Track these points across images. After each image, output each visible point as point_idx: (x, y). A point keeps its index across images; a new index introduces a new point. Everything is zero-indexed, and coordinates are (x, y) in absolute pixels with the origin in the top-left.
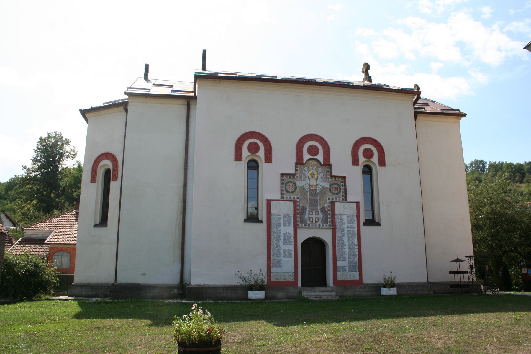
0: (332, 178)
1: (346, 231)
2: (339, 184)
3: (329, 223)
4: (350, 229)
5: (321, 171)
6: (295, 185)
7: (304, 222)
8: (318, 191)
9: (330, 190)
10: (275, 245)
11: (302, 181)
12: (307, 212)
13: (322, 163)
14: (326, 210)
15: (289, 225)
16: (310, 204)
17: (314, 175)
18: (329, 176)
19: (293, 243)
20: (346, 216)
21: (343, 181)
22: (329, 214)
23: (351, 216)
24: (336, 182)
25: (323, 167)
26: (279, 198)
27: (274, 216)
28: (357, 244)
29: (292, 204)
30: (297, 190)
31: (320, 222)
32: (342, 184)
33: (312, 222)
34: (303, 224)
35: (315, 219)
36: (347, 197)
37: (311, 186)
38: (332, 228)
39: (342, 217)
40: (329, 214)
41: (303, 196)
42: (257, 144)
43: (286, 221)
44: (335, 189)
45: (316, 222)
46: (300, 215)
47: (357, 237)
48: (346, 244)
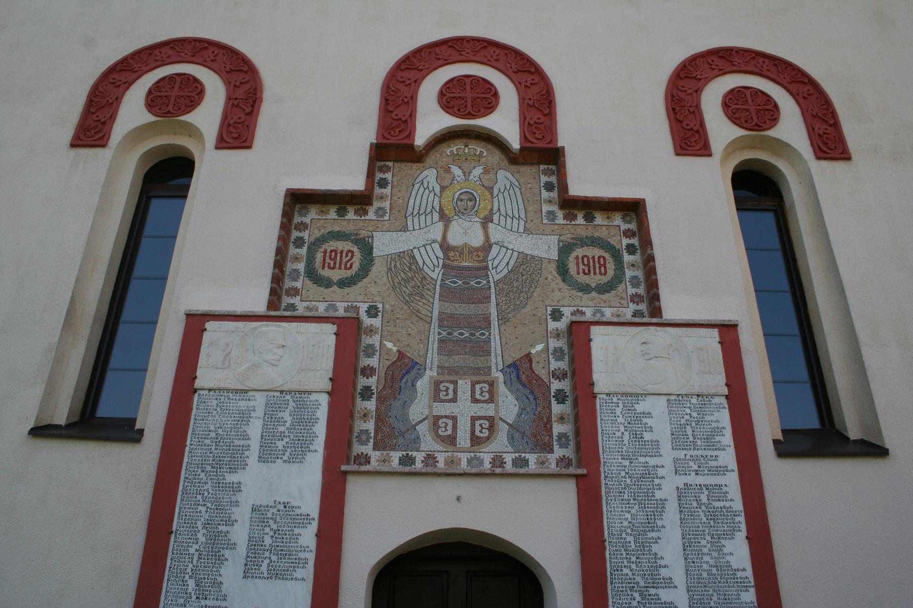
0: (570, 217)
1: (667, 490)
2: (613, 241)
3: (561, 446)
4: (692, 479)
5: (511, 184)
6: (367, 248)
7: (401, 441)
8: (495, 276)
9: (562, 269)
10: (191, 583)
11: (405, 229)
12: (423, 385)
13: (516, 145)
14: (542, 373)
15: (298, 454)
16: (441, 341)
17: (470, 204)
18: (555, 208)
19: (308, 572)
20: (663, 400)
21: (633, 226)
22: (561, 397)
23: (694, 400)
24: (596, 234)
25: (525, 169)
26: (260, 306)
27: (215, 402)
28: (749, 573)
29: (326, 335)
30: (373, 274)
31: (501, 442)
32: (625, 241)
33: (451, 440)
34: (396, 456)
35: (473, 425)
36: (658, 299)
37: (452, 254)
38: (577, 477)
39: (640, 407)
40: (568, 440)
41: (407, 303)
42: (196, 80)
43: (281, 429)
44: (588, 265)
45: (476, 441)
46: (381, 400)
47: (743, 526)
48: (677, 573)
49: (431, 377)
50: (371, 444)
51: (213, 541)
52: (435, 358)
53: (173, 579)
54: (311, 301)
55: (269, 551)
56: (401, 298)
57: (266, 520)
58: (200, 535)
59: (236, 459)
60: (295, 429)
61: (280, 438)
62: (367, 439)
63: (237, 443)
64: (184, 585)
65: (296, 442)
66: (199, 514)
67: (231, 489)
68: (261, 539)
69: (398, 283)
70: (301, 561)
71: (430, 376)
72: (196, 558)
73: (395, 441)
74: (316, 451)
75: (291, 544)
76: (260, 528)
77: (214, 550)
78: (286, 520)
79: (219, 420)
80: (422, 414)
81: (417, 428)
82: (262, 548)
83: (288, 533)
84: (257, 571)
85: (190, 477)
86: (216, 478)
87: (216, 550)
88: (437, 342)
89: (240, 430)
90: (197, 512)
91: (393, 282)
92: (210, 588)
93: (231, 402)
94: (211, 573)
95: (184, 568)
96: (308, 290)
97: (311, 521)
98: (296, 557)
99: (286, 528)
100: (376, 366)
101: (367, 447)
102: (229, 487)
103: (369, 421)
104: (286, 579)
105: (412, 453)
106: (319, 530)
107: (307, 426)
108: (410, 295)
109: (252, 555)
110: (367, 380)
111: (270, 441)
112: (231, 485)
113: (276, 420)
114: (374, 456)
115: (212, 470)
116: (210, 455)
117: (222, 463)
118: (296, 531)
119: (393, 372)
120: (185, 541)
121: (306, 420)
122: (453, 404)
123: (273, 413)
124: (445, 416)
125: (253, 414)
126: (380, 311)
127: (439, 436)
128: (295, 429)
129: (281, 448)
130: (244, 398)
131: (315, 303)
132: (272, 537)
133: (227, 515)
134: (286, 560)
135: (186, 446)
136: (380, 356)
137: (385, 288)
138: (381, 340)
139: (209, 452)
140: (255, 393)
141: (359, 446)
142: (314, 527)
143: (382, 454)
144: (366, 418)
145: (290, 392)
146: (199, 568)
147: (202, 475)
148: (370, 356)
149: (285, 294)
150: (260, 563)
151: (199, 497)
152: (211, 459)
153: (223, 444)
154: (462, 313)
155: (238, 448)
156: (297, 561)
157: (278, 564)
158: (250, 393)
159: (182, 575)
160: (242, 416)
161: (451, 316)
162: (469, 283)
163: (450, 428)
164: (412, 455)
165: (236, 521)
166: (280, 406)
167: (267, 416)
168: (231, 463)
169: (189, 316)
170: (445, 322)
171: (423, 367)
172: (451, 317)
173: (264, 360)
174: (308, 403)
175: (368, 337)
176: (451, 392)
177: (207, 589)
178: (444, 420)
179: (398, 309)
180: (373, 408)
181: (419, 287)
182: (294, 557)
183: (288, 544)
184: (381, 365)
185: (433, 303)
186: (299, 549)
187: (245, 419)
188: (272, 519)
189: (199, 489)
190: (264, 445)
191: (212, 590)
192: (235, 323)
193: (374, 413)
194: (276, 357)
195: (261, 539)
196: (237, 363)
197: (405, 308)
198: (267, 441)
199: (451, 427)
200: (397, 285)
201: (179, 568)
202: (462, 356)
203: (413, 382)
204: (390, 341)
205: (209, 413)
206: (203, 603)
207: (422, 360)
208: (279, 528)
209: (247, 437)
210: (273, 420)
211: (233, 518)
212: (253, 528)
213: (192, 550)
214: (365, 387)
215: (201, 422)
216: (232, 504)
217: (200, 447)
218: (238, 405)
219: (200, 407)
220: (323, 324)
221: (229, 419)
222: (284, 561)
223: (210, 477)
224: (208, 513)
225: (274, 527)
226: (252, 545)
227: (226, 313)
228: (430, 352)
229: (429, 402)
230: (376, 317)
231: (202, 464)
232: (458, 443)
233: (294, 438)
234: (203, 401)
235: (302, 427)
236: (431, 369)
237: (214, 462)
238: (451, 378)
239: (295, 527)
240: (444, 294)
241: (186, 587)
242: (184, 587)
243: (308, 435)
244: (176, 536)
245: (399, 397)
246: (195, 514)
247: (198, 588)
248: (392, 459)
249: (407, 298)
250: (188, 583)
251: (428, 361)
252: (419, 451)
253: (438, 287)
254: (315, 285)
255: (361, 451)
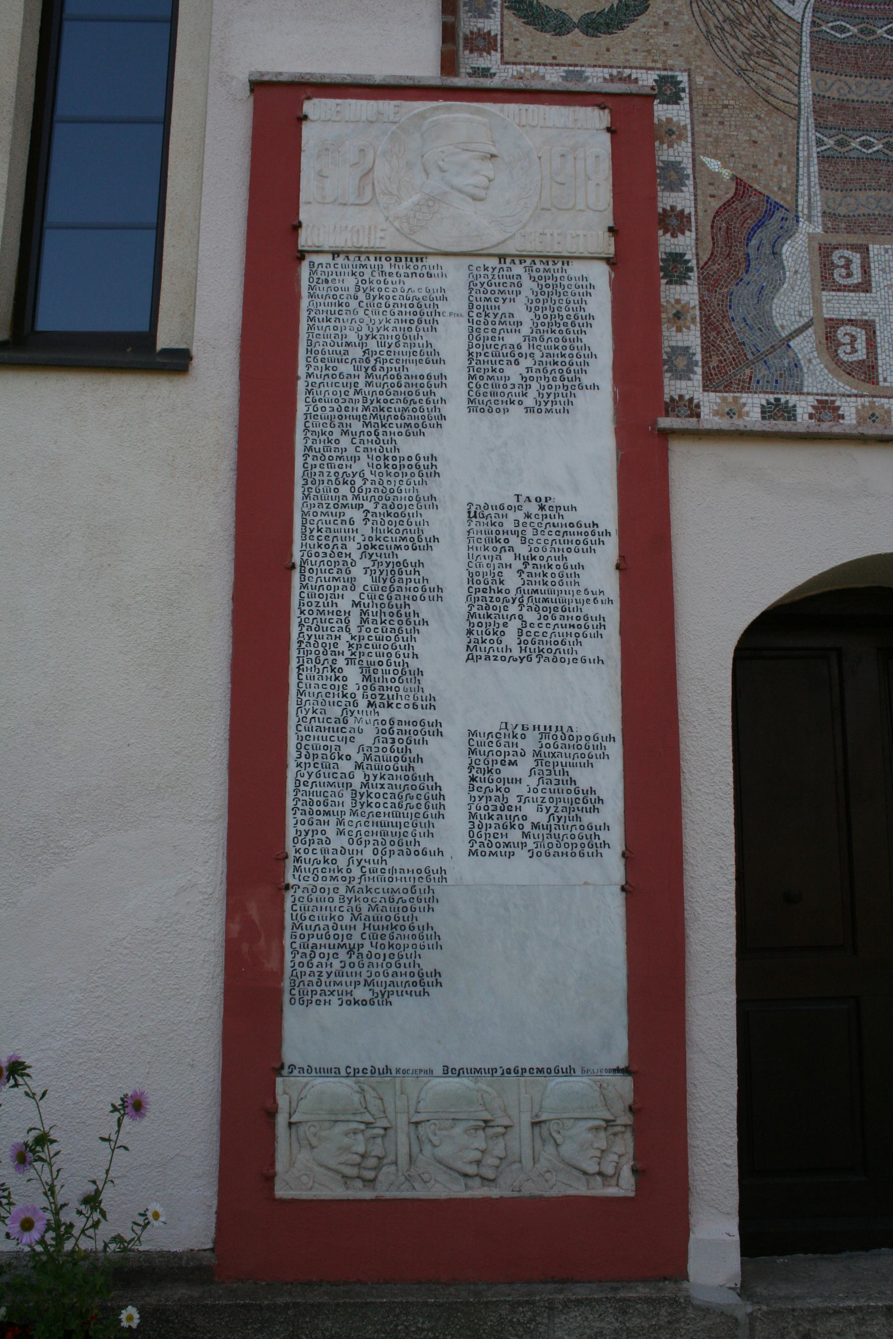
7: (761, 372)
10: (353, 674)
16: (823, 158)
27: (351, 282)
41: (741, 72)
43: (512, 339)
46: (708, 283)
49: (811, 237)
50: (698, 376)
51: (388, 584)
52: (816, 195)
53: (309, 666)
54: (526, 64)
55: (517, 602)
56: (728, 61)
57: (502, 537)
58: (357, 571)
59: (418, 406)
60: (542, 339)
61: (513, 360)
62: (687, 366)
63: (413, 369)
64: (337, 678)
65: (549, 368)
66: (348, 526)
67: (414, 470)
68: (497, 578)
69: (716, 27)
70: (590, 623)
71: (809, 234)
72: (355, 621)
73: (748, 371)
74: (595, 387)
75: (564, 588)
76: (490, 553)
77: (394, 602)
78: (547, 537)
79: (367, 320)
80: (800, 315)
81: (791, 344)
82: (501, 596)
83: (554, 563)
84: (495, 645)
85: (317, 446)
86: (378, 447)
87: (399, 602)
88: (816, 161)
89: (417, 342)
90: (343, 522)
91: (707, 25)
92: (397, 684)
93: (389, 279)
94: (393, 652)
95: (332, 642)
96: (516, 40)
97: (602, 538)
98: (579, 614)
99: (548, 554)
100: (689, 209)
101: (690, 383)
102: (410, 467)
103: (688, 328)
104: (563, 660)
105: (788, 397)
106: (622, 557)
107: (569, 333)
108: (747, 56)
109: (482, 612)
110: (673, 240)
111: (489, 366)
112: (414, 462)
113: (497, 320)
114: (707, 404)
115: (366, 430)
116: (357, 397)
117: (386, 414)
118: (573, 559)
119: (727, 223)
120: (325, 584)
121: (565, 320)
122: (862, 294)
123: (489, 304)
124: (850, 320)
125: (442, 306)
126: (683, 90)
127: (840, 363)
128: (542, 339)
129: (516, 379)
130: (418, 272)
131: (537, 68)
132: (520, 572)
133: (413, 527)
134: (558, 621)
135: (298, 378)
136: (695, 188)
137: (689, 39)
138: (693, 154)
139: (352, 391)
140: (440, 261)
141: (673, 382)
142: (610, 549)
143: (724, 399)
144: (681, 322)
145: (522, 258)
146: (366, 641)
147: (345, 441)
148: (675, 186)
149: (465, 48)
150: (501, 628)
151: (344, 490)
152: (360, 406)
153: (383, 373)
154: (865, 98)
155: (419, 381)
156: (582, 622)
157: (541, 631)
158: (431, 261)
159: (330, 658)
160: (418, 310)
161: (842, 105)
162: (874, 32)
163: (861, 344)
164: (787, 402)
165: (436, 539)
166: (502, 288)
167: (475, 310)
168: (406, 414)
169: (258, 86)
170: (830, 118)
171: (791, 216)
172: (842, 107)
173: (452, 187)
174: (566, 282)
175: (665, 146)
176: (856, 268)
177: (390, 684)
178: (849, 329)
179: (724, 87)
180: (695, 301)
181: (764, 37)
182: (575, 614)
183: (557, 587)
184: (700, 207)
185: (799, 75)
186: (583, 596)
187: (425, 317)
188: (516, 533)
189: (341, 471)
190: (478, 375)
191: (401, 686)
192: (372, 102)
193: (697, 312)
194: (481, 180)
195: (497, 578)
196: (391, 194)
197: (738, 84)
198: (482, 366)
199: (864, 344)
200: (714, 31)
201: (320, 642)
202: (873, 193)
203: (773, 246)
204: (715, 156)
205: (340, 305)
206: (385, 714)
207: (789, 198)
208: (534, 554)
209: (437, 357)
210: (490, 320)
211: (428, 533)
212: (476, 553)
213: (344, 605)
214: (670, 254)
215: (325, 324)
216: (422, 503)
217: (330, 381)
218: (406, 288)
219: (318, 292)
220: (577, 108)
221: (389, 317)
222: (553, 623)
223: (362, 446)
224: (369, 524)
225: (524, 550)
226: (477, 591)
227: (349, 80)
228: (803, 182)
229: (813, 290)
230: (677, 103)
231: (341, 417)
232: (881, 378)
233: (544, 359)
234: (323, 277)
235: (557, 335)
236: (809, 218)
237: (368, 413)
238: (853, 239)
239: (569, 550)
240: (821, 55)
241: (341, 683)
242: (337, 683)
243: (575, 352)
244: (302, 574)
245: (746, 278)
246: (340, 526)
247: (369, 684)
248: (746, 409)
249: (741, 62)
250: (344, 673)
251: (800, 201)
252: (801, 394)
253: (806, 39)
254: (530, 28)
255: (678, 392)
